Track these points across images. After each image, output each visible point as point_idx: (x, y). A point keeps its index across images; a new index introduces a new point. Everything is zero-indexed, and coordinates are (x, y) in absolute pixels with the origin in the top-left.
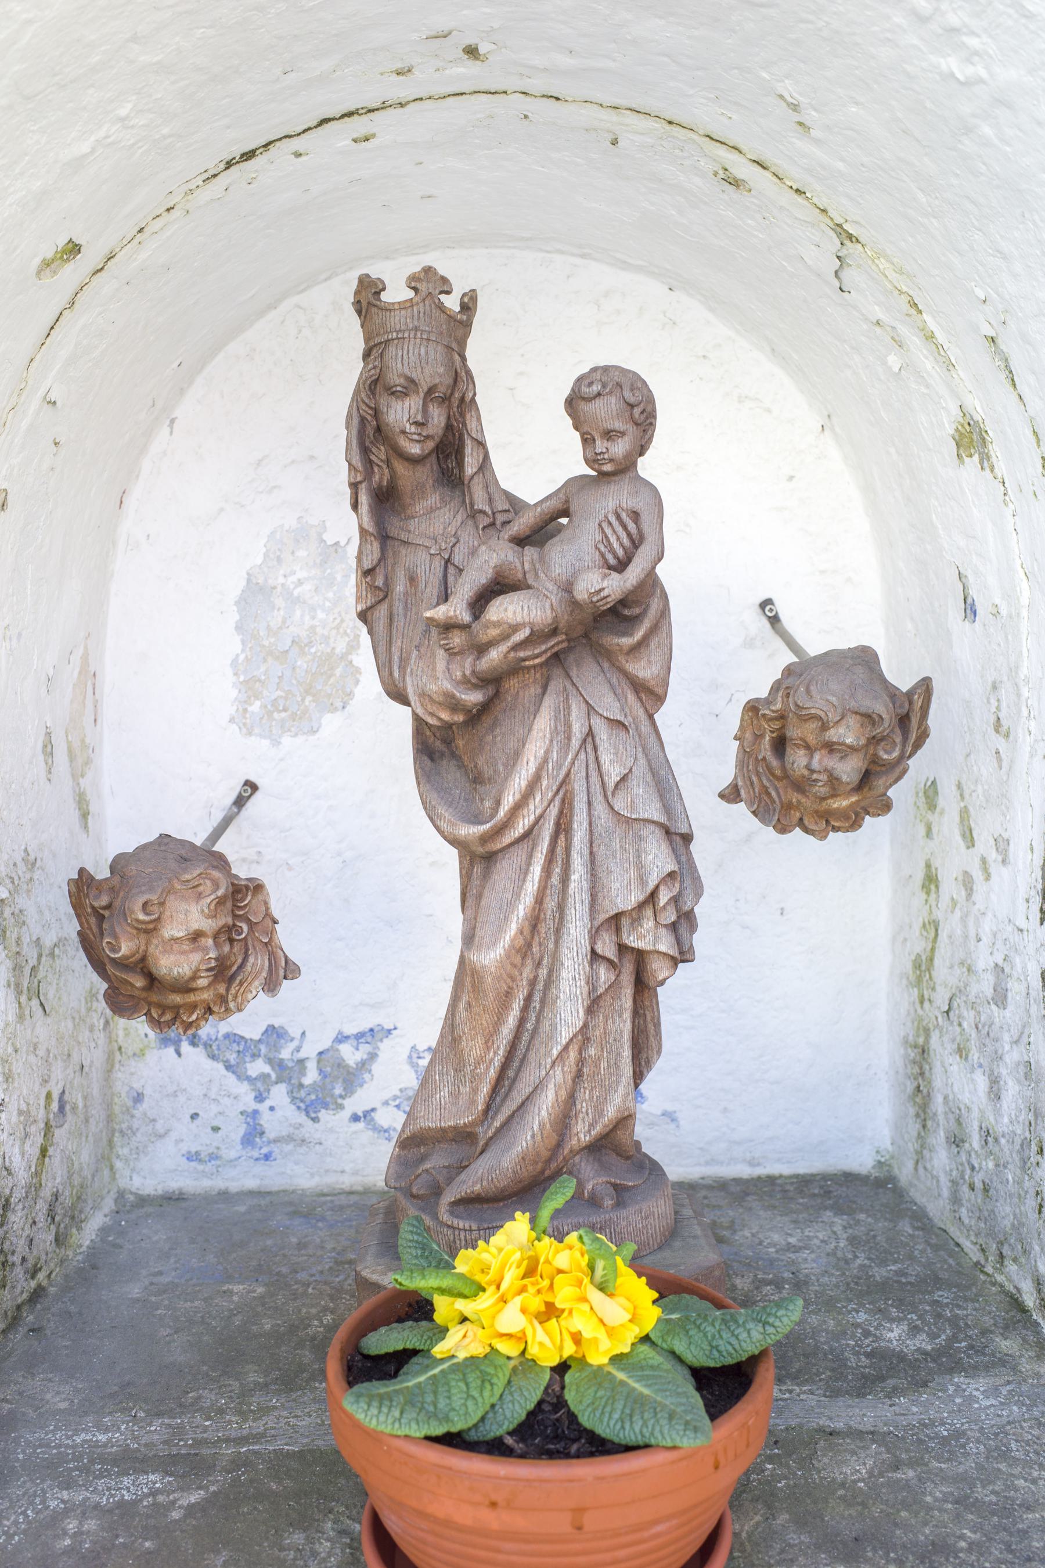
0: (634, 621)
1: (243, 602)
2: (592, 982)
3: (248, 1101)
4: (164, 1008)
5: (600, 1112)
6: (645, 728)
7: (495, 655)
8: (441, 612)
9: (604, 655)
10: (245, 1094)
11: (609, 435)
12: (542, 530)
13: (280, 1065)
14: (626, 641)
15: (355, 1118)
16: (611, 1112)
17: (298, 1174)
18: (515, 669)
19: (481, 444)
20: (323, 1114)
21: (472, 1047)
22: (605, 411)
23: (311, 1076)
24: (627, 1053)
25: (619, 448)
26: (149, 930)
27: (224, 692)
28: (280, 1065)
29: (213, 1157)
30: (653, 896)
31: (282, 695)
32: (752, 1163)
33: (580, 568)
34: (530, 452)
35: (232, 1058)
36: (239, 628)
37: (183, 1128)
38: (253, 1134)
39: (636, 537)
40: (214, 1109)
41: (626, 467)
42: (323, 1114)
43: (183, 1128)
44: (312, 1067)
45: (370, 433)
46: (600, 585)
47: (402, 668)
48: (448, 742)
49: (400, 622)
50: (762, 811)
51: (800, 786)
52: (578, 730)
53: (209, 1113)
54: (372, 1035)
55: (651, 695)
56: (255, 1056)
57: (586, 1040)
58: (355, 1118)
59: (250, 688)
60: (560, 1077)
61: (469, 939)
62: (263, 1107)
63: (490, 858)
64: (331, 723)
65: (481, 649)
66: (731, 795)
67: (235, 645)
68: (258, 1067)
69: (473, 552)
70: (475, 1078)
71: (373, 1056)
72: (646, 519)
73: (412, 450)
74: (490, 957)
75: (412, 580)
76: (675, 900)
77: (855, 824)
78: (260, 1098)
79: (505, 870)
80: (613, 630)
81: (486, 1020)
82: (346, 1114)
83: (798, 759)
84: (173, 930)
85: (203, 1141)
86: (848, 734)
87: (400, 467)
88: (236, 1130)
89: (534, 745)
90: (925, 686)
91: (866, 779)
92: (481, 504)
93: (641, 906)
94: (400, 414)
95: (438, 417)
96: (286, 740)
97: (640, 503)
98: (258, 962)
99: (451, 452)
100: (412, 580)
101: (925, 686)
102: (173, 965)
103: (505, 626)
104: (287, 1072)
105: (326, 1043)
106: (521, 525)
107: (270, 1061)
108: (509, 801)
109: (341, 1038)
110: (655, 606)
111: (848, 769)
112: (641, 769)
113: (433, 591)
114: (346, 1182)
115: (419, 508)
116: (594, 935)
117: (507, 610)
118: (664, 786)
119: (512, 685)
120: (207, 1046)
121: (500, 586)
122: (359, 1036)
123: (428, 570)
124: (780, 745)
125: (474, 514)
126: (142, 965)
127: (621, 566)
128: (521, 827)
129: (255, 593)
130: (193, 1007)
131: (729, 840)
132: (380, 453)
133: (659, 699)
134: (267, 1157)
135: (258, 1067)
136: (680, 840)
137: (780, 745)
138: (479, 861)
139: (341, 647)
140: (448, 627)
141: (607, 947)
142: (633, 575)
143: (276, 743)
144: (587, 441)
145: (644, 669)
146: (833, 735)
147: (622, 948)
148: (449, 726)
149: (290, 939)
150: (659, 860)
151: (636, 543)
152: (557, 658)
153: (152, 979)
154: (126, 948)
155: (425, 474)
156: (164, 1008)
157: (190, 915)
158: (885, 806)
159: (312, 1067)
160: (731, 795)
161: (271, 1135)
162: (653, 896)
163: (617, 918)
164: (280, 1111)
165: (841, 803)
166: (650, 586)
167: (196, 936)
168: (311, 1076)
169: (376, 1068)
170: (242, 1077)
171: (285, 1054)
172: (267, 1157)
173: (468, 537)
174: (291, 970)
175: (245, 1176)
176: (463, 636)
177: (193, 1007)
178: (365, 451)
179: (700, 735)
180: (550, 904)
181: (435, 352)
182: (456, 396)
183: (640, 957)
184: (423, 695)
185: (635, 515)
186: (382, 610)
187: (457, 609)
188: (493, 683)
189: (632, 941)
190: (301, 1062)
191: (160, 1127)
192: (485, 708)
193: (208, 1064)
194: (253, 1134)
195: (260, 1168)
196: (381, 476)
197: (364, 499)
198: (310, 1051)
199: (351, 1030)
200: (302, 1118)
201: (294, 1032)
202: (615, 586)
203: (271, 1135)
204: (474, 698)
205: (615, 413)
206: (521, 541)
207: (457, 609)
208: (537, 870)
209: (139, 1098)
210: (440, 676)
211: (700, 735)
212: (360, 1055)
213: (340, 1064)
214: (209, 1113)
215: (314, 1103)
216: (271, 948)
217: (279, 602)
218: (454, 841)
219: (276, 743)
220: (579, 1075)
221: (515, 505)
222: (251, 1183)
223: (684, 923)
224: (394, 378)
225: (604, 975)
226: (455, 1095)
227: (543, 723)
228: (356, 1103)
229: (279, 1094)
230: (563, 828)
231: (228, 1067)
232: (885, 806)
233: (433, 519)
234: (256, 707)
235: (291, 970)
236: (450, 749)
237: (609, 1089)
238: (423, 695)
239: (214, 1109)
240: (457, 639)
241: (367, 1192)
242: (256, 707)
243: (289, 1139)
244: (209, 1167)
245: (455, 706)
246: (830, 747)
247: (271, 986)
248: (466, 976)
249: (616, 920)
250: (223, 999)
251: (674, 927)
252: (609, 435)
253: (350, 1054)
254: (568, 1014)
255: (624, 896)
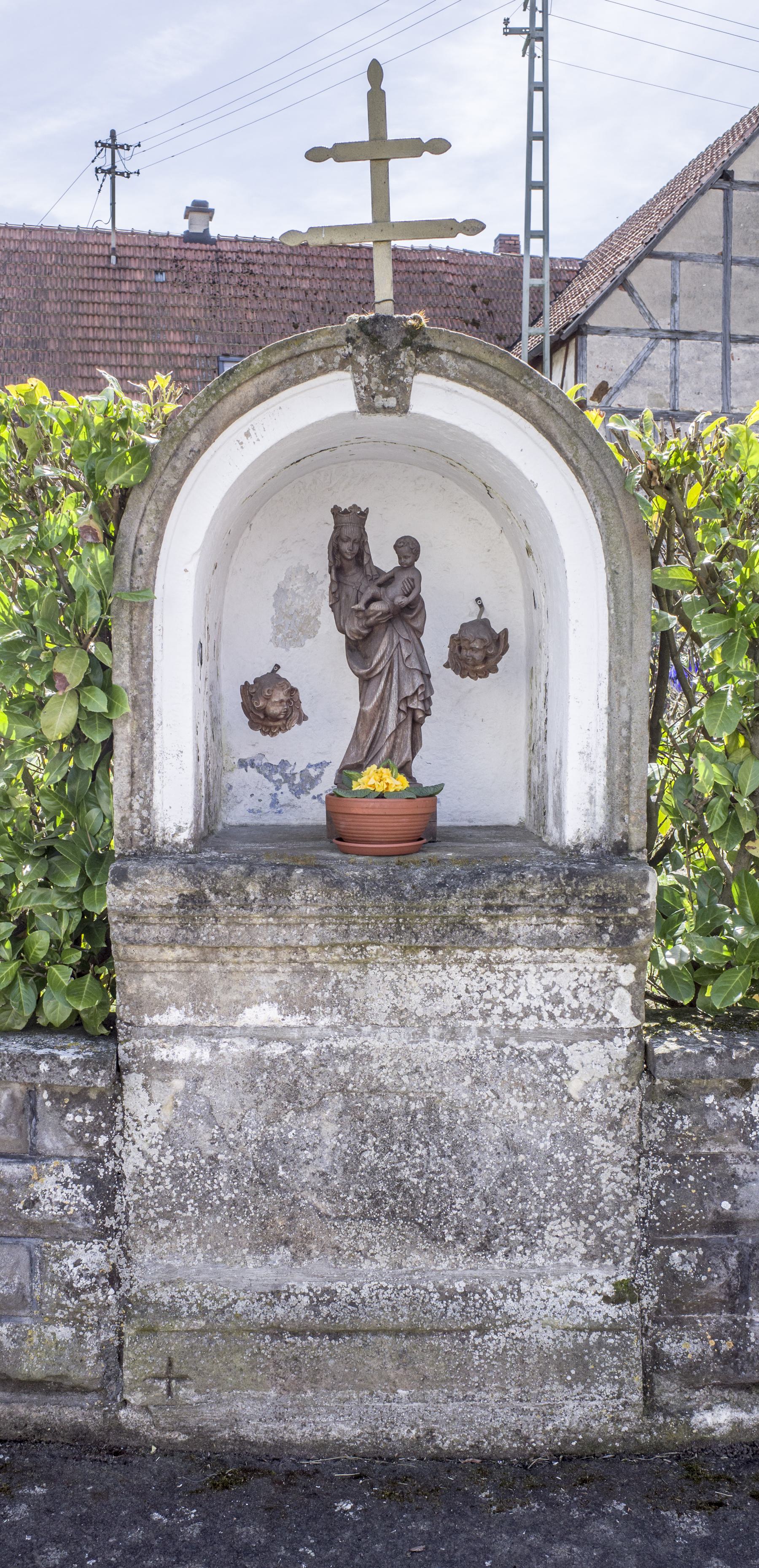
0: (413, 610)
1: (276, 595)
2: (398, 720)
3: (273, 790)
4: (267, 727)
5: (400, 759)
6: (416, 642)
7: (372, 619)
8: (356, 607)
9: (404, 620)
10: (271, 786)
11: (405, 557)
12: (390, 580)
13: (285, 776)
14: (410, 616)
15: (314, 798)
16: (404, 759)
17: (291, 818)
18: (377, 624)
19: (369, 555)
20: (302, 796)
21: (362, 738)
22: (405, 550)
23: (298, 780)
24: (409, 741)
25: (408, 561)
26: (268, 699)
27: (268, 629)
28: (285, 776)
29: (259, 811)
30: (417, 691)
31: (293, 629)
32: (470, 821)
33: (396, 595)
34: (384, 559)
35: (267, 773)
36: (274, 605)
37: (247, 800)
38: (275, 803)
39: (415, 582)
40: (260, 792)
41: (411, 565)
42: (302, 796)
43: (247, 800)
44: (298, 777)
45: (335, 551)
46: (402, 600)
47: (344, 622)
48: (357, 646)
49: (343, 608)
50: (456, 671)
51: (465, 661)
52: (395, 642)
53: (258, 794)
54: (322, 765)
55: (419, 632)
56: (276, 772)
57: (396, 737)
58: (314, 798)
59: (278, 629)
60: (388, 745)
61: (362, 705)
62: (279, 792)
63: (368, 681)
64: (309, 643)
65: (368, 618)
66: (447, 666)
67: (272, 612)
68: (277, 777)
69: (366, 588)
70: (363, 748)
71: (322, 773)
72: (416, 582)
73: (347, 554)
74: (368, 708)
75: (347, 596)
76: (424, 693)
77: (486, 676)
78: (277, 789)
79: (373, 683)
80: (409, 613)
81: (367, 728)
82: (311, 796)
83: (464, 652)
84: (275, 699)
85: (255, 805)
86: (477, 645)
87: (345, 562)
88: (268, 801)
89: (383, 647)
90: (505, 631)
91: (485, 660)
92: (369, 573)
93: (414, 695)
94: (345, 547)
95: (356, 548)
96: (291, 649)
97: (414, 576)
98: (295, 714)
99: (361, 556)
100: (347, 596)
101: (505, 631)
102: (275, 710)
103: (30, 1428)
104: (288, 779)
105: (304, 767)
106: (382, 579)
107: (281, 774)
108: (375, 662)
109: (310, 766)
110: (419, 605)
111: (478, 656)
112: (414, 654)
113: (353, 600)
114: (310, 822)
115: (350, 573)
116: (399, 703)
117: (376, 606)
118: (422, 660)
119: (376, 628)
120: (258, 768)
121: (374, 599)
122: (317, 765)
123: (352, 592)
124: (460, 649)
125: (366, 576)
126: (264, 710)
127: (407, 595)
128: (379, 670)
129: (281, 592)
130: (275, 727)
131: (444, 680)
132: (338, 557)
133: (421, 633)
134: (280, 812)
135: (277, 777)
136: (426, 676)
137: (460, 649)
138: (365, 681)
139: (313, 613)
140: (358, 611)
141: (403, 708)
142: (412, 597)
143: (288, 650)
144: (400, 558)
145: (417, 624)
146: (472, 645)
147: (408, 708)
148: (357, 641)
149: (305, 708)
150: (418, 681)
151: (413, 588)
152: (390, 621)
153: (266, 715)
154: (261, 704)
155: (352, 564)
156: (267, 727)
157: (280, 695)
158: (496, 670)
159: (298, 777)
160: (447, 666)
161: (281, 803)
162: (417, 691)
163: (406, 698)
164: (285, 794)
165: (480, 668)
166: (419, 599)
167: (281, 701)
168: (298, 780)
169: (323, 778)
170: (270, 780)
171: (288, 772)
172: (280, 812)
173: (364, 584)
174: (306, 718)
175: (271, 819)
176: (364, 614)
177: (275, 727)
178: (334, 556)
179: (436, 644)
180: (387, 694)
181: (356, 529)
182: (362, 541)
183: (414, 711)
184: (350, 631)
185: (413, 580)
186: (338, 605)
187: (361, 606)
188: (371, 627)
189: (411, 706)
190: (294, 774)
191: (238, 799)
192: (368, 635)
193: (258, 775)
194: (275, 803)
195: (277, 816)
196: (338, 563)
197: (333, 571)
198: (298, 770)
199: (313, 763)
200: (293, 797)
201: (292, 763)
202: (405, 601)
203: (281, 803)
204: (365, 632)
205: (408, 549)
206: (380, 585)
207: (361, 606)
208: (383, 683)
209: (230, 787)
210: (355, 626)
211: (436, 644)
212: (317, 773)
213: (309, 776)
214: (258, 794)
215: (298, 791)
216: (300, 710)
217: (290, 595)
218: (358, 675)
219: (288, 650)
220: (394, 747)
221: (379, 572)
222: (273, 822)
223: (427, 701)
224: (344, 537)
225: (402, 716)
226: (357, 754)
227: (385, 640)
228: (315, 792)
229: (285, 787)
230: (390, 671)
231: (265, 776)
232: (496, 670)
233: (354, 577)
234: (280, 636)
235: (306, 718)
236: (357, 649)
237: (403, 752)
238: (350, 631)
239: (260, 792)
240: (361, 615)
241: (318, 826)
242: (280, 636)
243: (289, 805)
244: (257, 815)
245: (359, 634)
246: (472, 649)
247: (299, 722)
248: (362, 714)
249: (406, 699)
250: (285, 726)
251: (423, 701)
252: (405, 557)
253: (313, 772)
254: (391, 726)
255: (408, 691)
